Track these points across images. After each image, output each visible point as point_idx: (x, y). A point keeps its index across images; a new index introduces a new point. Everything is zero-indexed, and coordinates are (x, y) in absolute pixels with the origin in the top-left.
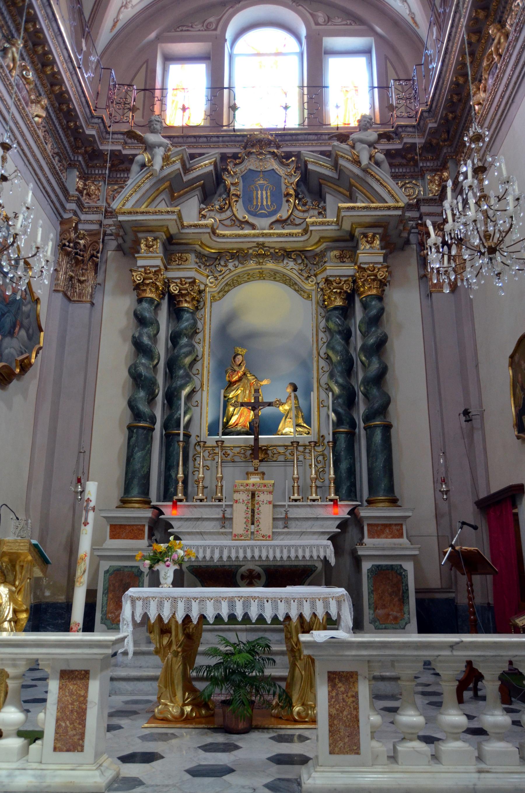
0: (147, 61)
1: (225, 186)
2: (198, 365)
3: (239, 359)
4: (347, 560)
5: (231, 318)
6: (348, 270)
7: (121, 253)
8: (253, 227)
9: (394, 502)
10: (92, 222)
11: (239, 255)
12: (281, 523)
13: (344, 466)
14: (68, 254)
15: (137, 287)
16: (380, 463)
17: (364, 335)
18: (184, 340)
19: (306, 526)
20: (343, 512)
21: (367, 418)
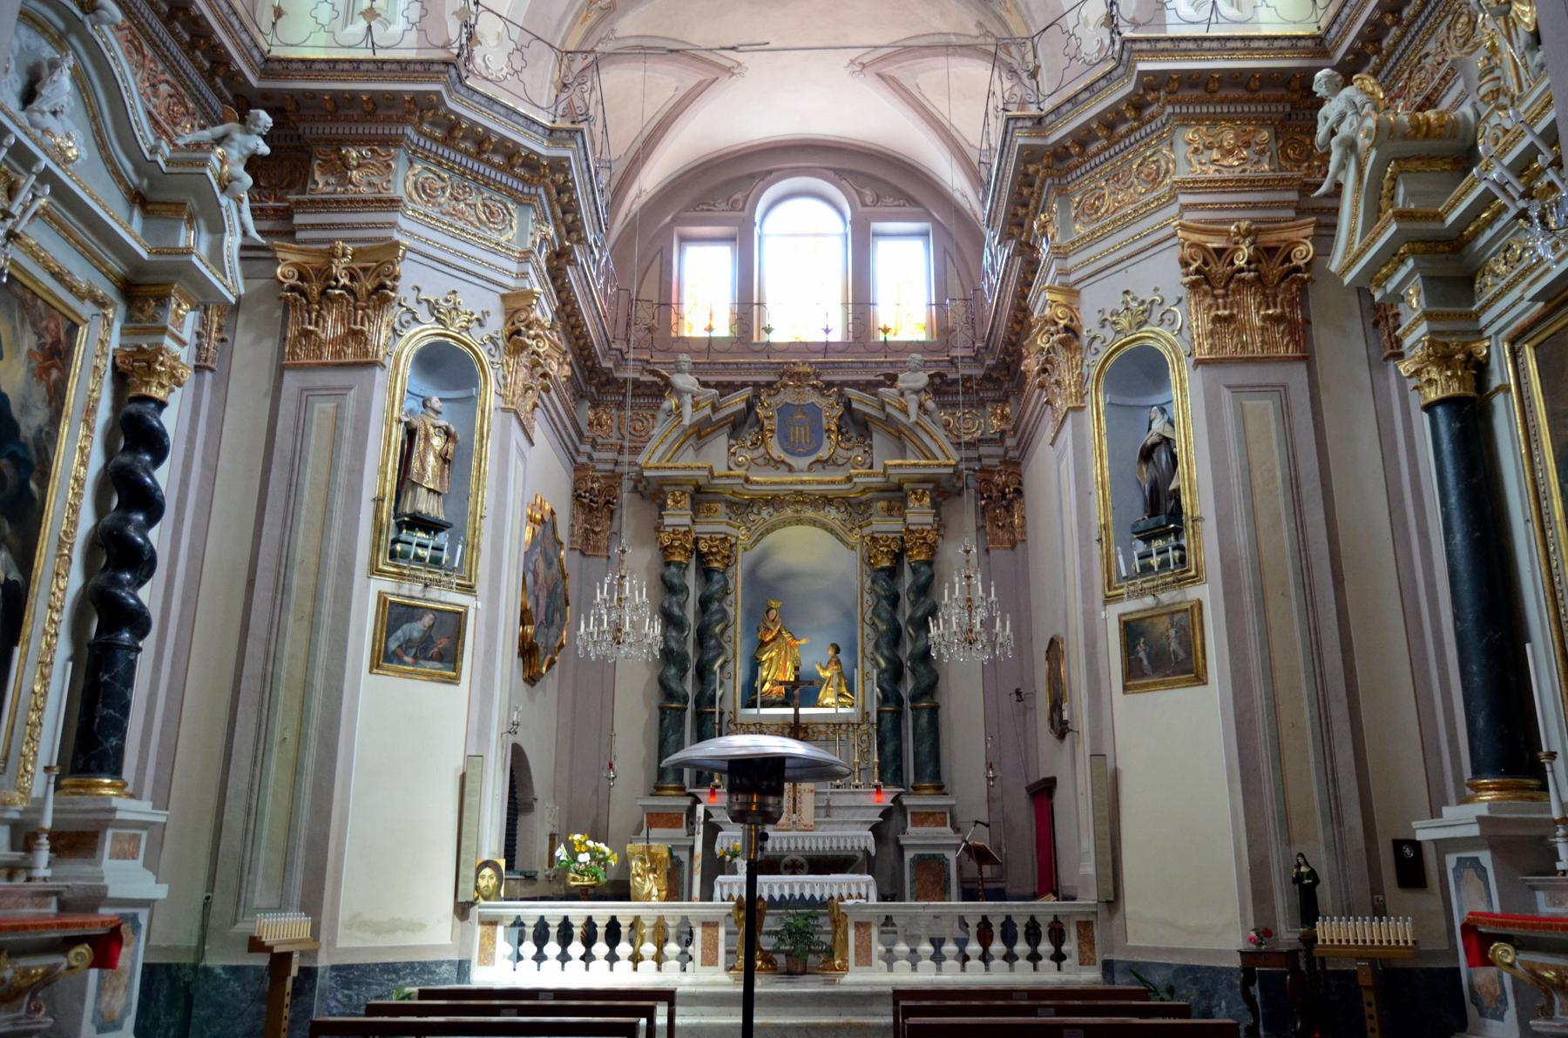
0: (661, 250)
1: (758, 420)
2: (730, 632)
3: (773, 613)
4: (890, 850)
5: (763, 557)
6: (895, 525)
7: (638, 496)
8: (791, 469)
9: (940, 789)
10: (606, 461)
11: (775, 502)
12: (822, 812)
13: (889, 748)
14: (583, 505)
15: (664, 549)
16: (925, 748)
17: (914, 604)
18: (715, 606)
19: (847, 815)
20: (887, 800)
21: (914, 699)
